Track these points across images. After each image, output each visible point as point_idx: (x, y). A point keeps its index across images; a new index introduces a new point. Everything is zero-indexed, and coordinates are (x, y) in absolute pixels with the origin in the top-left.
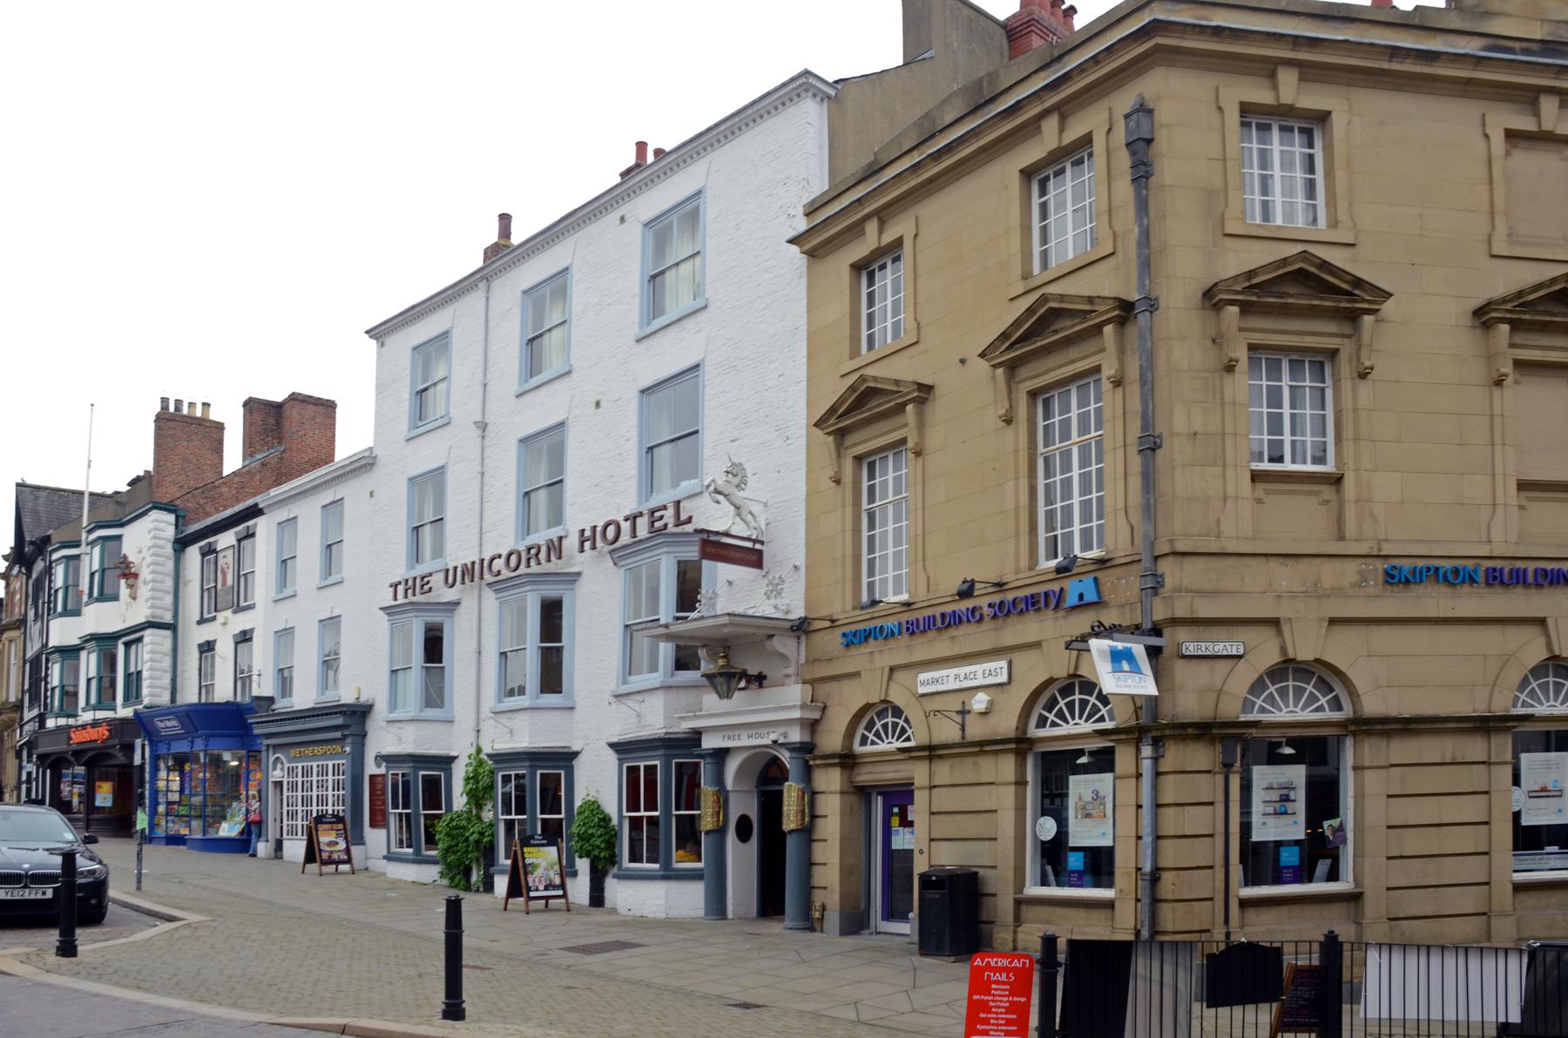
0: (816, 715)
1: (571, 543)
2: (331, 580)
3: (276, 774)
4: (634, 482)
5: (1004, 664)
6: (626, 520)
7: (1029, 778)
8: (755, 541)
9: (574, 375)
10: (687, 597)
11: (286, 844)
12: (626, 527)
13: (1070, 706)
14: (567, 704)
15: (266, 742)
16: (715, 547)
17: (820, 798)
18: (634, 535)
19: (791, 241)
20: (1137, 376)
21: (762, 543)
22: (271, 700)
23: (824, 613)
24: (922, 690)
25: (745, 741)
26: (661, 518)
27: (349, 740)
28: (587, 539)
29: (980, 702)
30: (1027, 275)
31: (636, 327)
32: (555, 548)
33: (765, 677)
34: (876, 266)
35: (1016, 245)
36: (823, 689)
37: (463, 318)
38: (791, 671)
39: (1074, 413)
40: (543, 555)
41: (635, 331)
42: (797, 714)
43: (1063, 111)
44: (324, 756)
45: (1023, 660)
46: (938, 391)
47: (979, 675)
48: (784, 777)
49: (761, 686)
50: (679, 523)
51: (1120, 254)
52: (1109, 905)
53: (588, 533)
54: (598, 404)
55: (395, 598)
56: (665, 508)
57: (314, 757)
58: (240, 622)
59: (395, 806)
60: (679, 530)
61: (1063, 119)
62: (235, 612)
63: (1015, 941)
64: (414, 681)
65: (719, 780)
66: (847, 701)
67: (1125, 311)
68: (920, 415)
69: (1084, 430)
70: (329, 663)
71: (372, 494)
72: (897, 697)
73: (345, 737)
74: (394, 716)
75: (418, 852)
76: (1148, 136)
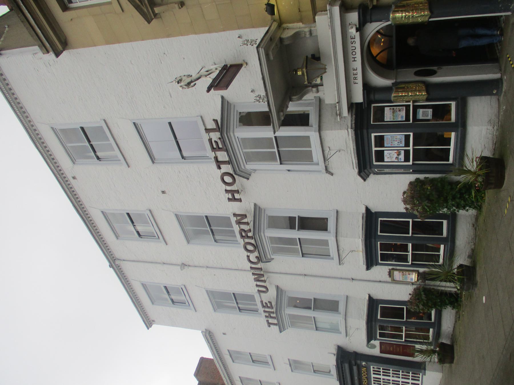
1: (236, 207)
2: (270, 363)
6: (219, 168)
9: (152, 209)
27: (359, 362)
28: (234, 196)
32: (241, 218)
37: (137, 274)
54: (163, 192)
64: (324, 317)
71: (224, 334)
73: (356, 364)
74: (342, 329)
75: (453, 127)
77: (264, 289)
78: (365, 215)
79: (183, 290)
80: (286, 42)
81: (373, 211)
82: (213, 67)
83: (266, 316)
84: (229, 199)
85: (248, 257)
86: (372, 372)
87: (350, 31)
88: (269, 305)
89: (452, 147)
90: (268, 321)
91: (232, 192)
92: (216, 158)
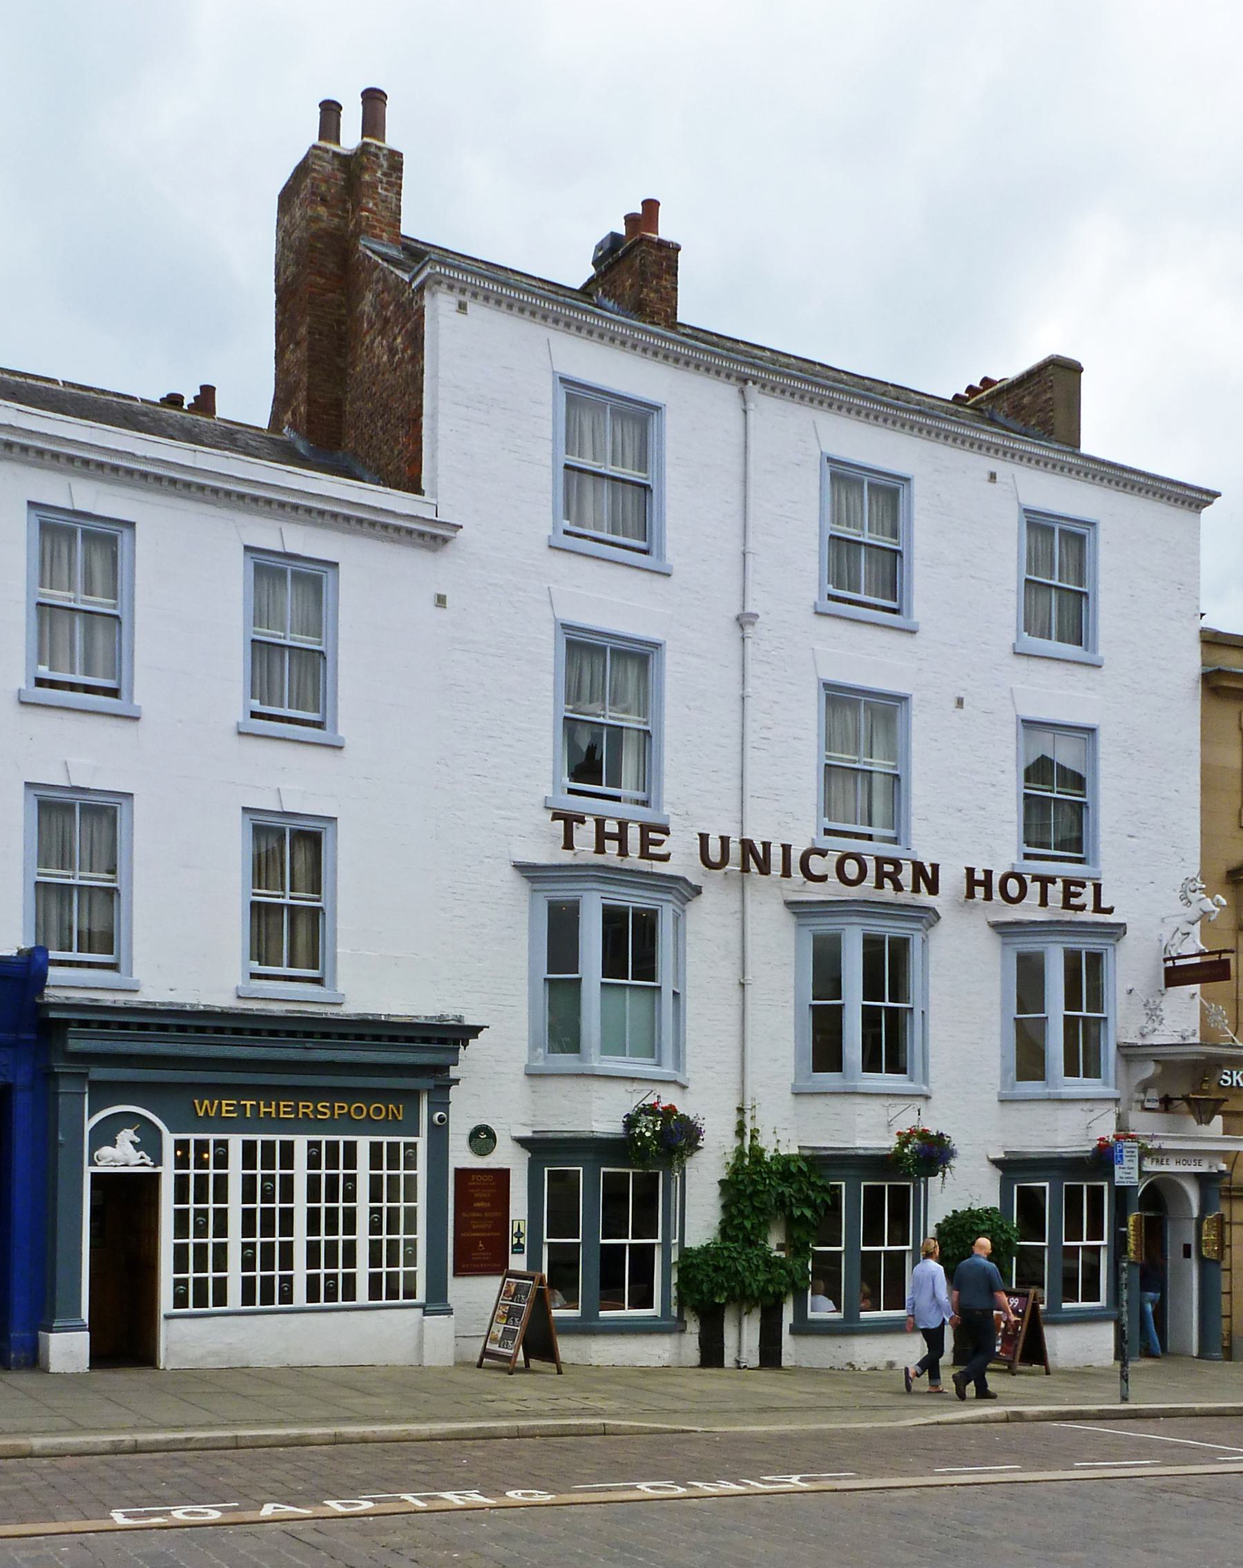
6: (1035, 878)
50: (1098, 909)
53: (979, 876)
60: (645, 865)
84: (970, 871)
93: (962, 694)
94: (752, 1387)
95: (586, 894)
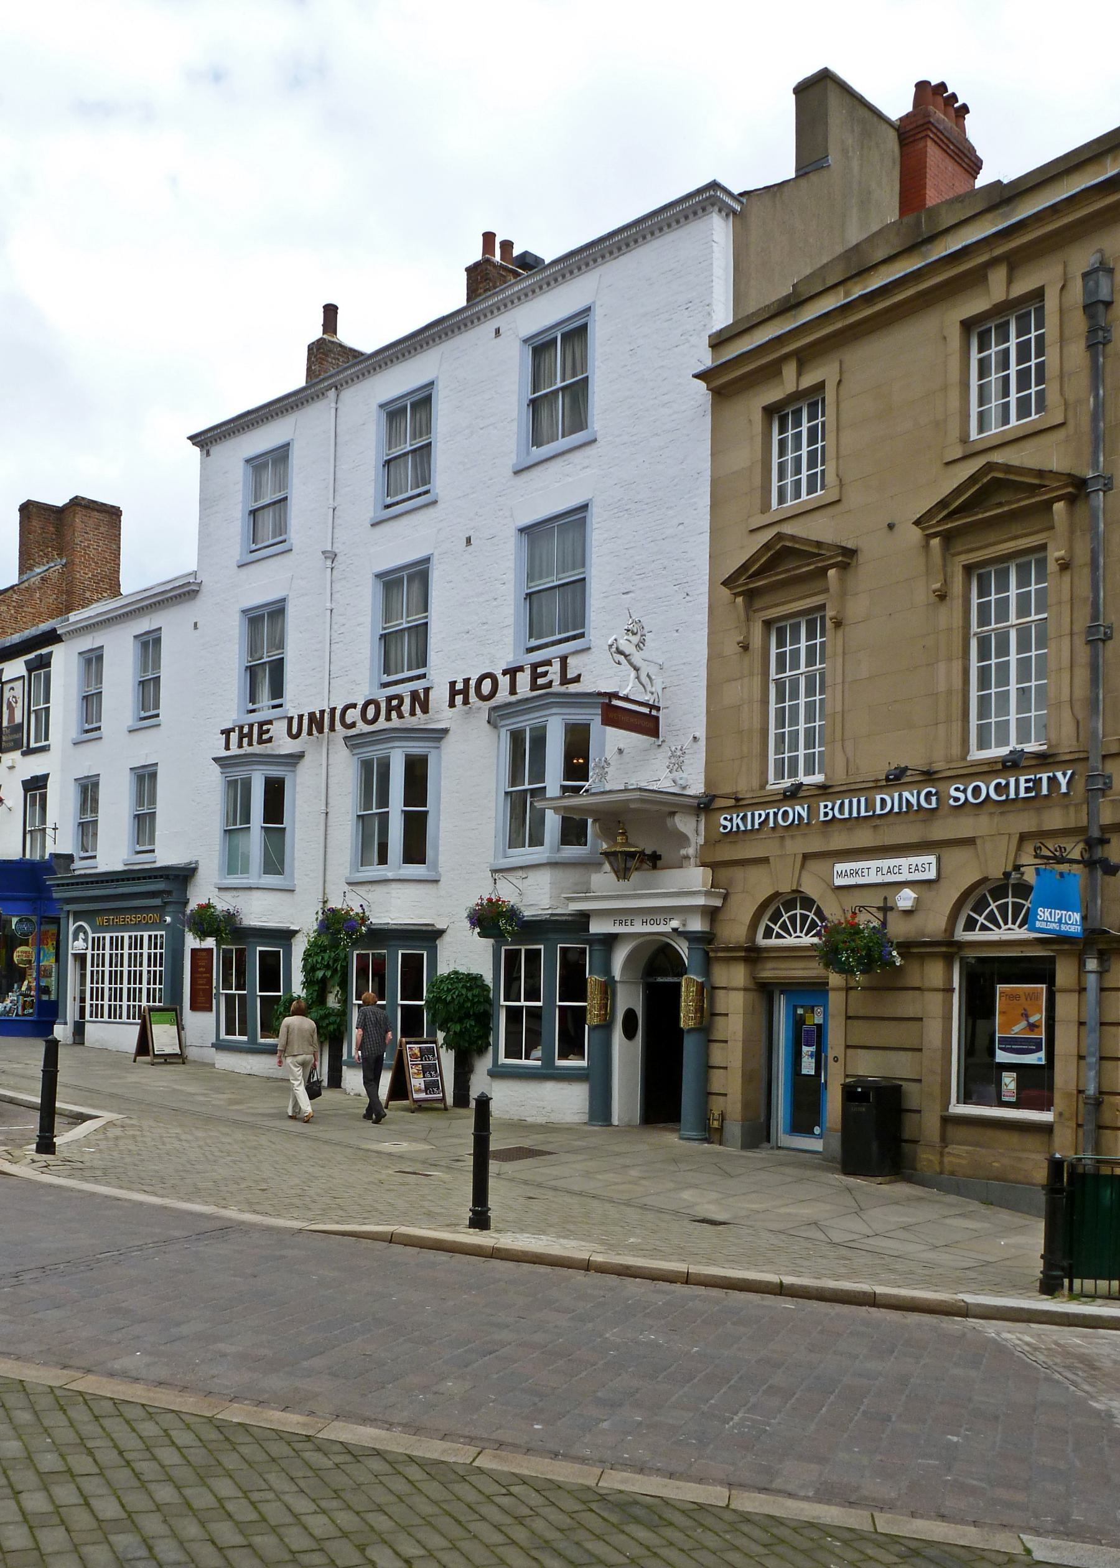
0: (718, 903)
3: (77, 946)
4: (510, 631)
5: (932, 859)
6: (505, 673)
7: (956, 985)
8: (651, 707)
10: (577, 767)
11: (88, 1026)
12: (504, 681)
13: (1003, 909)
14: (432, 875)
15: (67, 907)
16: (614, 712)
17: (720, 994)
18: (513, 691)
19: (696, 376)
20: (1088, 559)
21: (658, 709)
22: (70, 858)
23: (727, 789)
24: (839, 882)
25: (638, 928)
26: (545, 674)
27: (170, 909)
28: (458, 693)
29: (906, 899)
30: (964, 439)
31: (514, 456)
32: (421, 701)
33: (659, 857)
34: (789, 410)
35: (954, 403)
36: (724, 874)
37: (302, 431)
38: (691, 851)
39: (1013, 592)
40: (406, 708)
41: (511, 460)
42: (701, 901)
43: (1014, 262)
44: (138, 926)
45: (956, 857)
46: (862, 558)
47: (905, 870)
48: (680, 969)
49: (655, 867)
50: (565, 681)
51: (1071, 423)
52: (1046, 1129)
53: (459, 686)
54: (469, 541)
55: (227, 748)
56: (548, 663)
57: (125, 928)
58: (33, 766)
59: (227, 985)
60: (563, 689)
61: (1012, 270)
62: (24, 754)
63: (941, 1163)
65: (607, 969)
66: (755, 887)
67: (1078, 489)
68: (842, 580)
69: (1023, 611)
70: (144, 824)
72: (810, 888)
76: (1108, 299)
77: (295, 730)
78: (430, 928)
79: (280, 545)
80: (669, 822)
81: (438, 942)
82: (658, 687)
83: (241, 728)
84: (453, 684)
85: (354, 706)
86: (153, 933)
87: (303, 994)
88: (265, 737)
89: (524, 1062)
90: (233, 730)
91: (465, 692)
92: (521, 669)
93: (471, 533)
94: (132, 1078)
95: (549, 718)
